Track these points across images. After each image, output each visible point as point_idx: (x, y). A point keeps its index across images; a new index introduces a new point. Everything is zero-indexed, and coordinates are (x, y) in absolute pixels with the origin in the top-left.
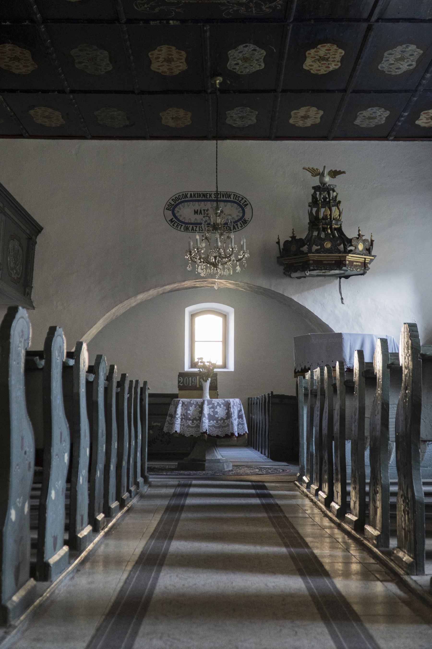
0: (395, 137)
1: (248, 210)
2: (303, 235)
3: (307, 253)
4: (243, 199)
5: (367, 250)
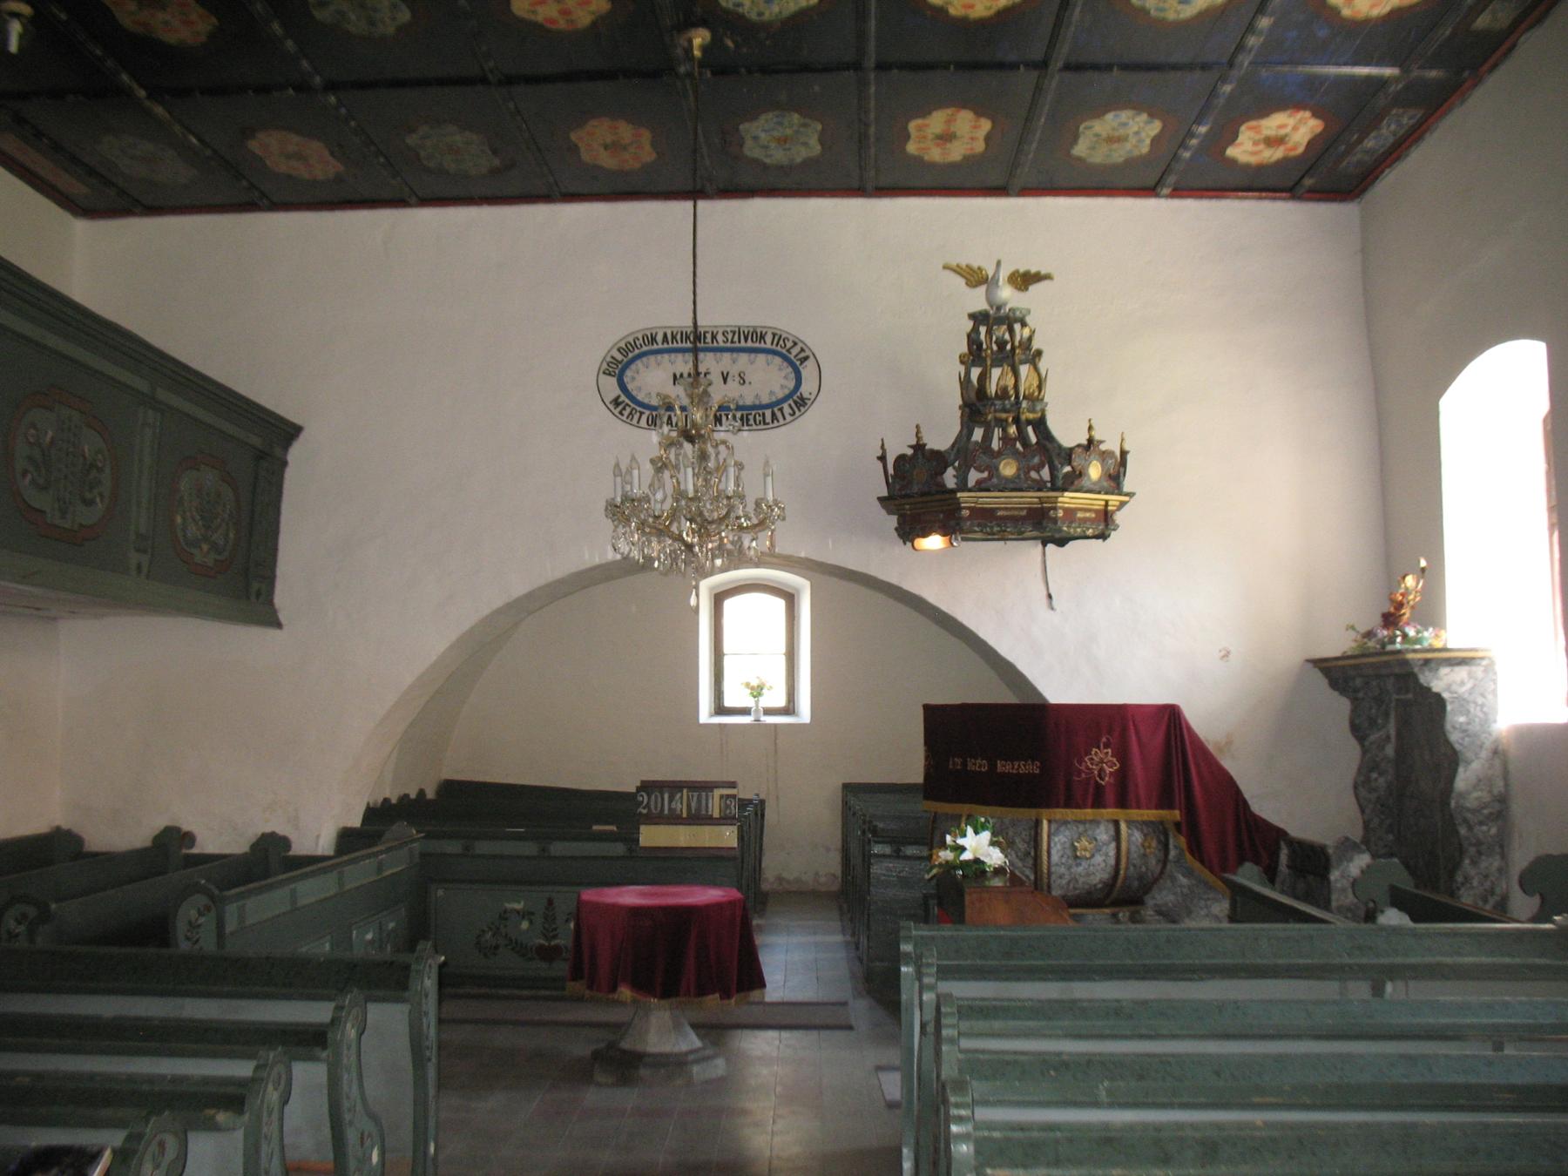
0: (1175, 190)
1: (808, 371)
2: (941, 438)
3: (953, 491)
4: (795, 344)
5: (1111, 477)
